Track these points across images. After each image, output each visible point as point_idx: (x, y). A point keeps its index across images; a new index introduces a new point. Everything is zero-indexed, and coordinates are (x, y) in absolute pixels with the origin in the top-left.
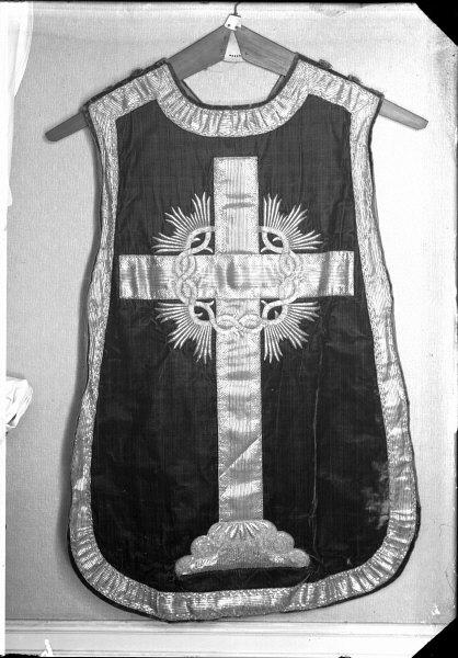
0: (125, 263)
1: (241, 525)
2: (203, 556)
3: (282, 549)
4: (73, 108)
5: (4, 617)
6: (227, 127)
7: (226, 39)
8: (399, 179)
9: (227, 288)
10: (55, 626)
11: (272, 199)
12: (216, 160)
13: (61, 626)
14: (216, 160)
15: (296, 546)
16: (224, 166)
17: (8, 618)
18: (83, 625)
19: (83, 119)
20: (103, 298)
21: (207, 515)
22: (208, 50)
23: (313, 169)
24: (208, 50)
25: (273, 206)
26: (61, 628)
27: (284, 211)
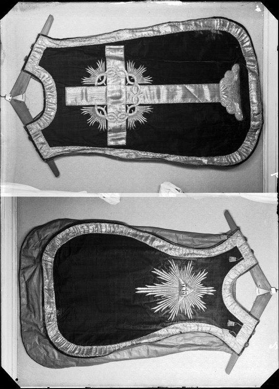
2: (234, 109)
4: (45, 166)
6: (53, 100)
7: (15, 100)
8: (76, 25)
16: (69, 101)
17: (17, 197)
21: (217, 107)
23: (70, 64)
25: (86, 80)
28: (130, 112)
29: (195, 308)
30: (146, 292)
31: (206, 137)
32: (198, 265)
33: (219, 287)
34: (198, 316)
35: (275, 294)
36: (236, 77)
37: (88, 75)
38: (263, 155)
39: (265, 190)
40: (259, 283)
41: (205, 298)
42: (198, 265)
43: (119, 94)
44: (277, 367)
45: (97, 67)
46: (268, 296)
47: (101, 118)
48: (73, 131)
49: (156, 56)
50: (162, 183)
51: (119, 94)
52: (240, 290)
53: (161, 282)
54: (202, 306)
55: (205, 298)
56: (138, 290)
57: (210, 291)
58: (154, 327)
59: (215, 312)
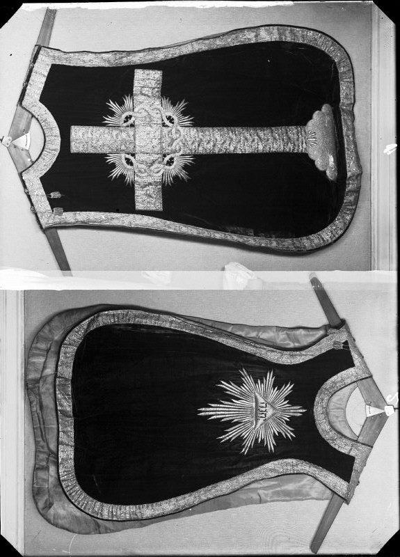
0: (139, 206)
1: (312, 140)
2: (325, 162)
3: (319, 121)
4: (42, 237)
5: (26, 289)
6: (55, 144)
7: (378, 407)
8: (86, 37)
9: (149, 106)
10: (374, 247)
11: (106, 120)
12: (72, 152)
13: (374, 243)
14: (72, 152)
15: (320, 110)
16: (76, 147)
17: (27, 293)
18: (374, 230)
19: (50, 232)
20: (84, 61)
21: (303, 160)
22: (375, 397)
23: (81, 93)
24: (375, 397)
25: (109, 120)
26: (376, 243)
27: (112, 114)
28: (131, 117)
29: (279, 438)
30: (231, 418)
31: (288, 206)
32: (283, 374)
33: (309, 404)
34: (284, 449)
35: (391, 413)
36: (328, 119)
37: (112, 114)
38: (372, 223)
39: (374, 267)
40: (24, 153)
41: (292, 422)
42: (283, 374)
43: (150, 138)
44: (397, 529)
45: (123, 103)
46: (382, 418)
47: (128, 170)
48: (83, 186)
49: (209, 81)
50: (228, 263)
51: (150, 138)
52: (344, 410)
53: (230, 398)
54: (289, 432)
55: (292, 422)
56: (201, 412)
57: (298, 411)
58: (255, 463)
59: (309, 445)
